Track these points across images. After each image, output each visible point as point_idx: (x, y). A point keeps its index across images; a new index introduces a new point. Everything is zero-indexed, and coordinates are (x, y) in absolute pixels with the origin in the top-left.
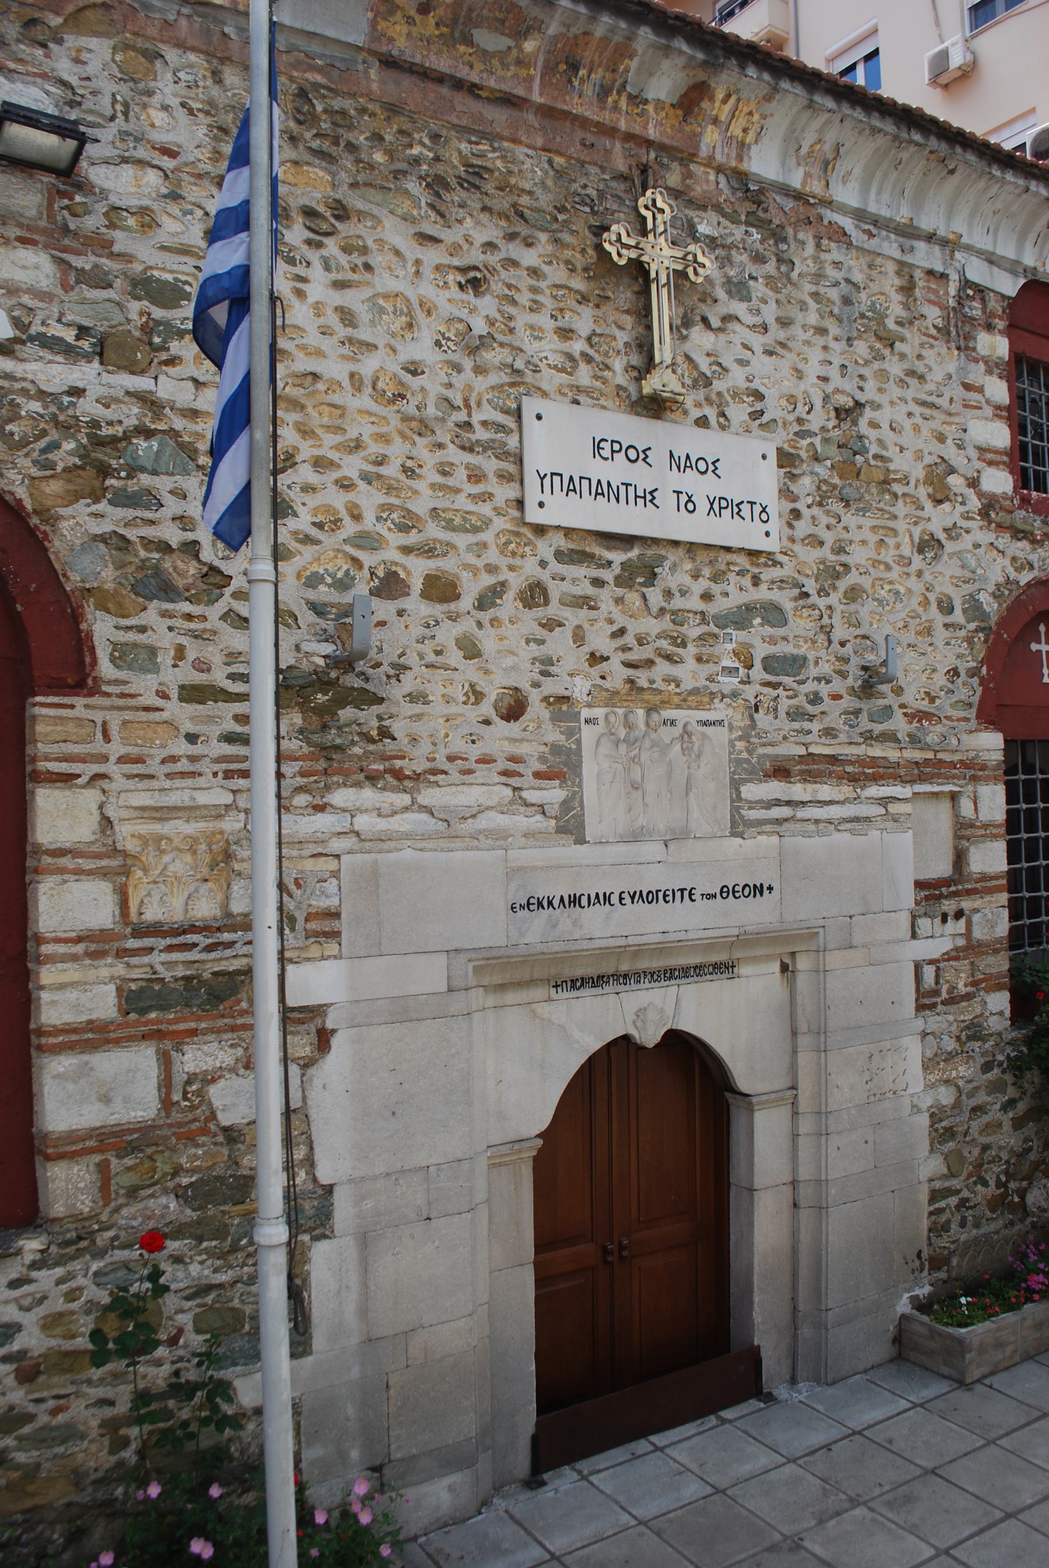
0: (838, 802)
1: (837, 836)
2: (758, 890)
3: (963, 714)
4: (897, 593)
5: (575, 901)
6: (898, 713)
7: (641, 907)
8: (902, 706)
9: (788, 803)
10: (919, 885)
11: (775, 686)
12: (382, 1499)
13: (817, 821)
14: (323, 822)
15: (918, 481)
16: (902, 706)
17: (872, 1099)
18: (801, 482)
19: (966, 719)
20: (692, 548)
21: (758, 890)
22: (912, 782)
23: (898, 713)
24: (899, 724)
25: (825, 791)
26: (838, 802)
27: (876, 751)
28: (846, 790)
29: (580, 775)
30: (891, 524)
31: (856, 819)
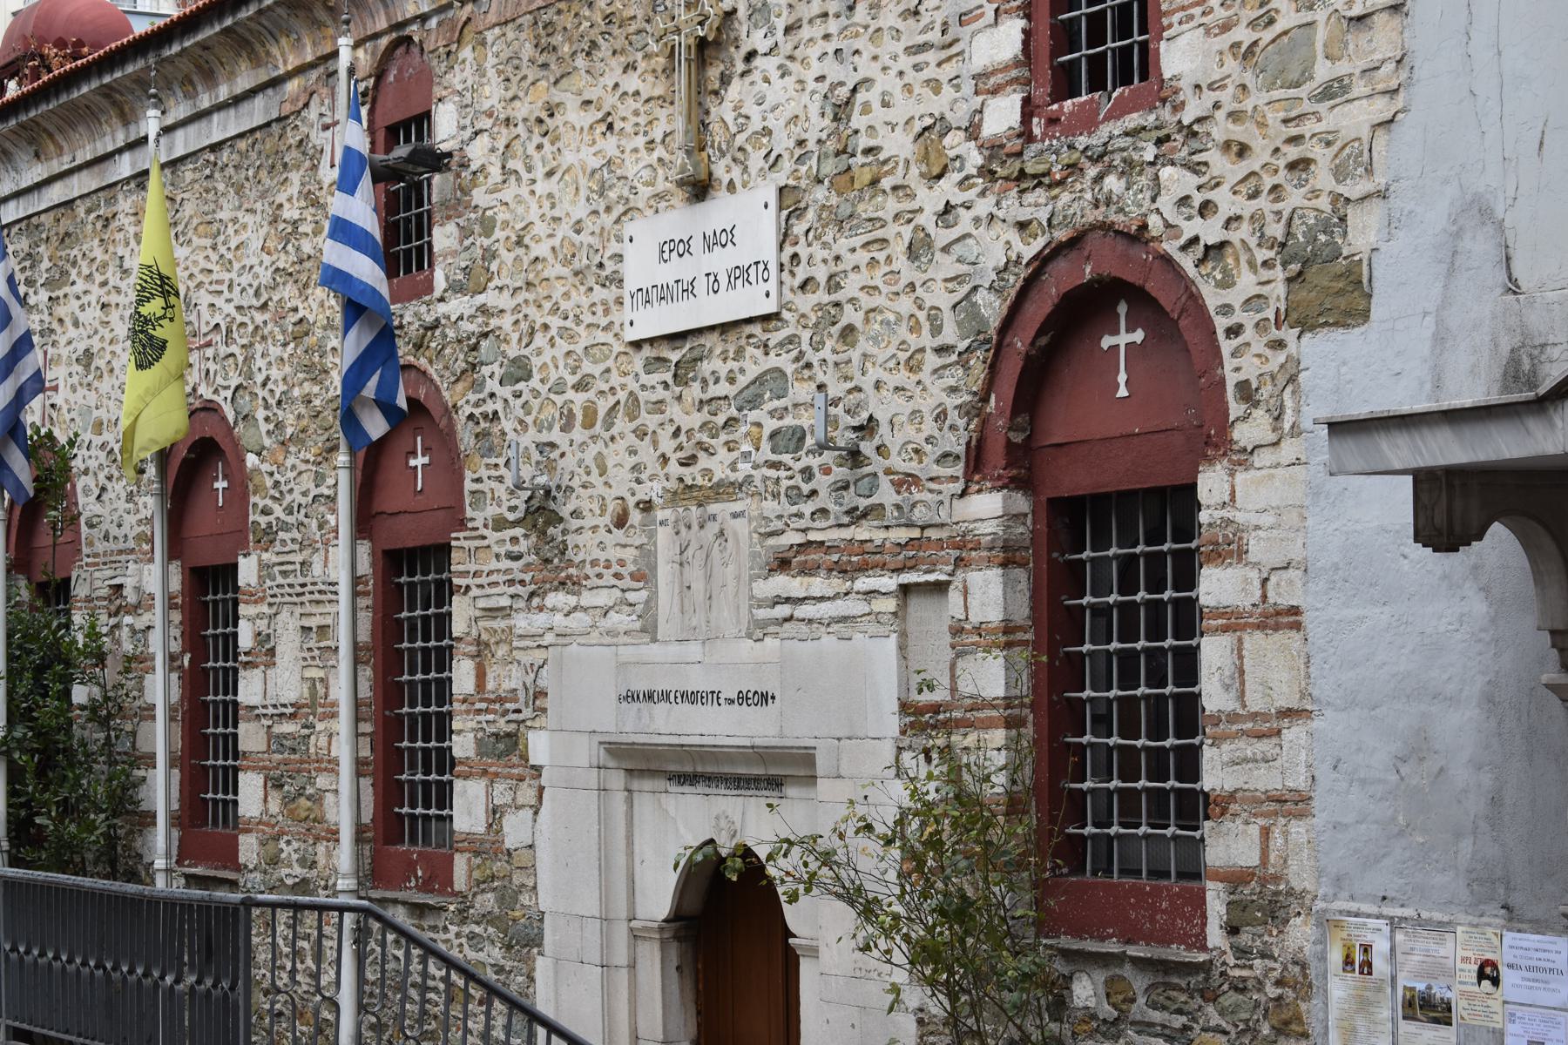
0: (829, 598)
1: (826, 639)
2: (765, 698)
3: (949, 471)
4: (888, 323)
5: (650, 696)
6: (885, 482)
7: (660, 687)
8: (888, 472)
9: (788, 600)
10: (905, 707)
11: (775, 465)
12: (188, 389)
13: (810, 621)
14: (541, 620)
15: (907, 162)
16: (888, 472)
17: (858, 974)
18: (1150, 224)
19: (954, 479)
20: (724, 328)
21: (765, 698)
22: (897, 571)
23: (885, 482)
24: (886, 495)
25: (818, 585)
26: (829, 598)
27: (861, 532)
28: (837, 584)
29: (655, 576)
30: (879, 234)
31: (844, 619)
